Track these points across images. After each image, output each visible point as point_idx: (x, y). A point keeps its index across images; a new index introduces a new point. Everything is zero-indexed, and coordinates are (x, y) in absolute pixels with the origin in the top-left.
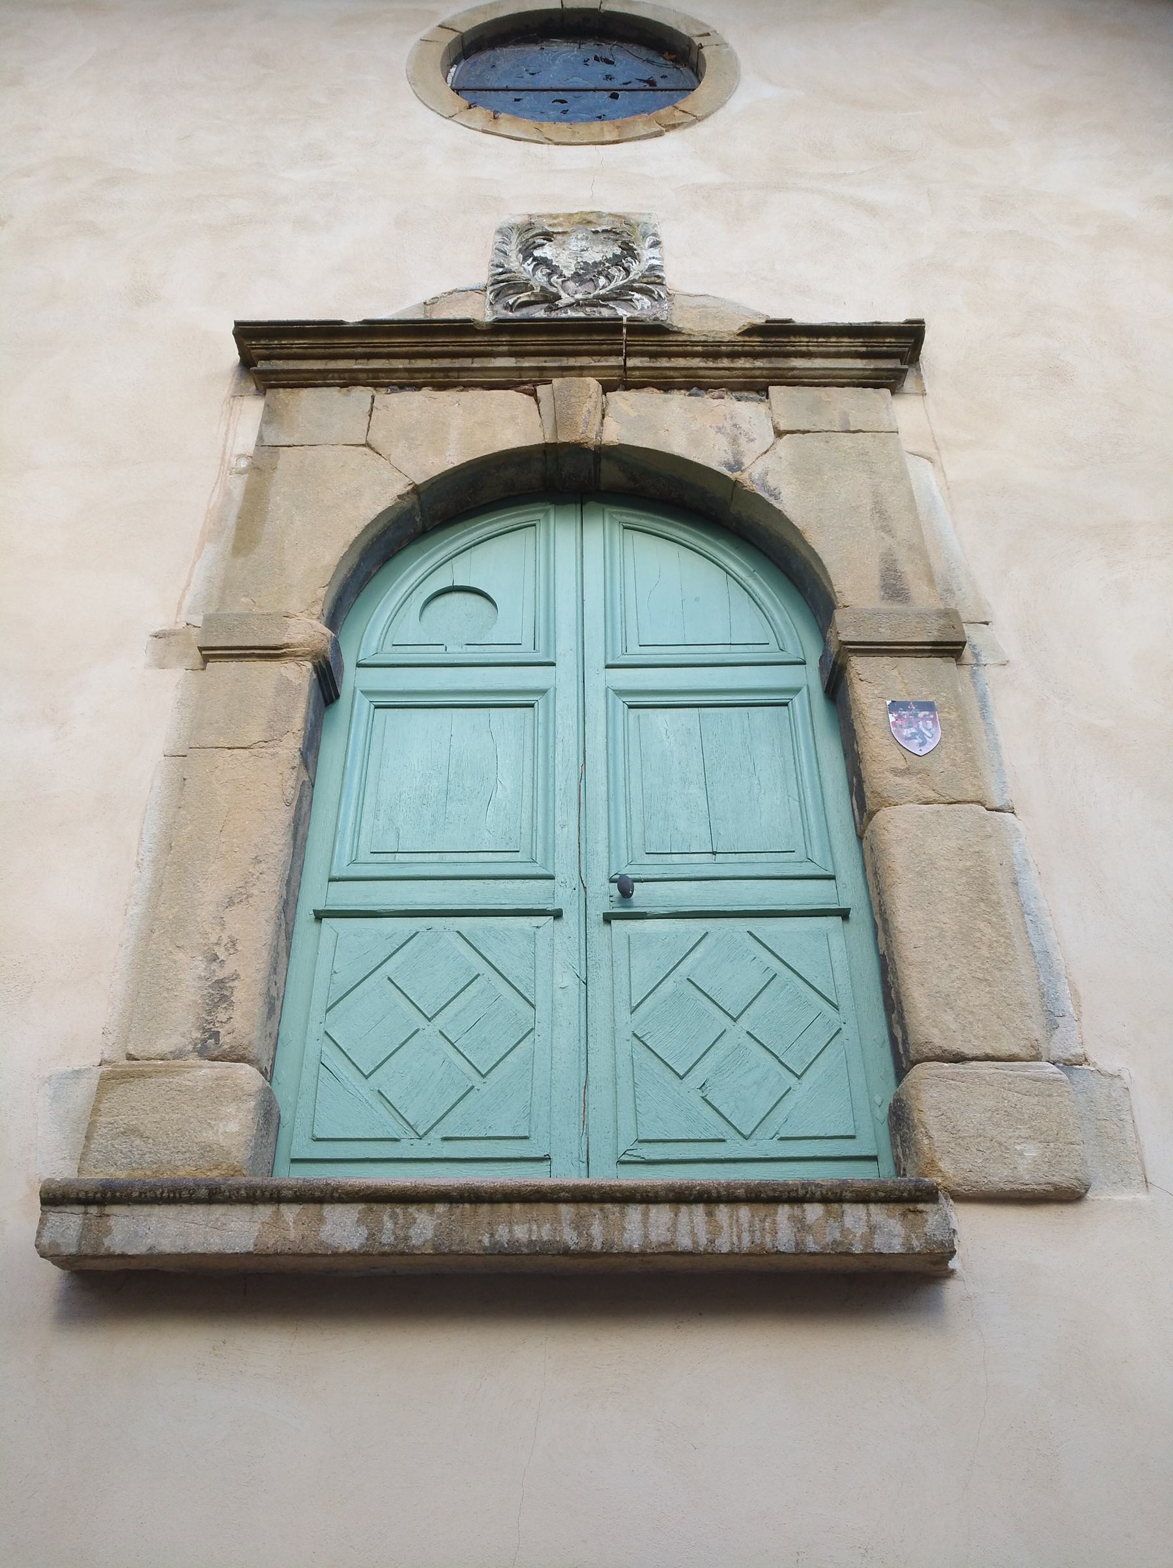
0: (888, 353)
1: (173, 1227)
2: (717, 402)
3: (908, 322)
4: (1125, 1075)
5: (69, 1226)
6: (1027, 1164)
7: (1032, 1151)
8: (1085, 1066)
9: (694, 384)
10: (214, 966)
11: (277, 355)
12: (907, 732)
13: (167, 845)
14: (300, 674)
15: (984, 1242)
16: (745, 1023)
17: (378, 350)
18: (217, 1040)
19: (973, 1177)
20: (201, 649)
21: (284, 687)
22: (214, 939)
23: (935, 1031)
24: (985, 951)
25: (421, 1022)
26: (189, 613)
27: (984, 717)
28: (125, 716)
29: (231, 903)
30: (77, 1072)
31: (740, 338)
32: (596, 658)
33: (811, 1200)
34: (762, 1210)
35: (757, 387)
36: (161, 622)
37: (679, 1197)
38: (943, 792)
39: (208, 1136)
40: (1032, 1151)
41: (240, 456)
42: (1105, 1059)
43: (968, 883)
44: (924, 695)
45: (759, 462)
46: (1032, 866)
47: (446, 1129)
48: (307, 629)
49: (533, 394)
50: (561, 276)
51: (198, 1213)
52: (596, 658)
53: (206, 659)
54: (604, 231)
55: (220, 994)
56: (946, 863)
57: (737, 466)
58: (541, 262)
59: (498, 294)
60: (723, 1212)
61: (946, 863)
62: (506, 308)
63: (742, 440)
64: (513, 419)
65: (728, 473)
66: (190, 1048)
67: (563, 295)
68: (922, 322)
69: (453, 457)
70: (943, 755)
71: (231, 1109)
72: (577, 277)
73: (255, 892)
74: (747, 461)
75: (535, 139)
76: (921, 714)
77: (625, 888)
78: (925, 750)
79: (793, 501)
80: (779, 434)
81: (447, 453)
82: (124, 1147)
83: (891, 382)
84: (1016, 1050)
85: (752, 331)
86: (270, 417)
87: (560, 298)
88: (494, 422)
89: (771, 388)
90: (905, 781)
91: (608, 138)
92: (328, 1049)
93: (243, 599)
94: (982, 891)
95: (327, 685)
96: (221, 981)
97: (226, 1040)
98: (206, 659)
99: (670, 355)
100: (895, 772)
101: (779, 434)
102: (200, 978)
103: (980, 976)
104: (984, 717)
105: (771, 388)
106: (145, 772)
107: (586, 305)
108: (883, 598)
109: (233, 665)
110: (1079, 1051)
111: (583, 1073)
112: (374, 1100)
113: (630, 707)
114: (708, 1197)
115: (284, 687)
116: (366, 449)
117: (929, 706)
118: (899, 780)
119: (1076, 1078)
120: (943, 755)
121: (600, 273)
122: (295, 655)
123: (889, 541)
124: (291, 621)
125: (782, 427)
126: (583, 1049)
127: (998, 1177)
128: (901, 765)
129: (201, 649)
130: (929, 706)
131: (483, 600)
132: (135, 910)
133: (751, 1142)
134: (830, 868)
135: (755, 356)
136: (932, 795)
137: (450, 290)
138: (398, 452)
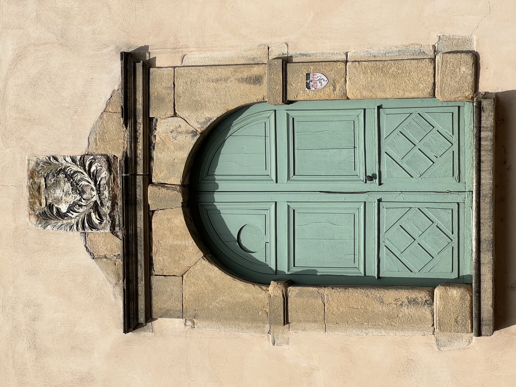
1: (486, 302)
2: (157, 138)
3: (122, 59)
4: (439, 35)
7: (463, 69)
8: (436, 46)
9: (149, 146)
10: (404, 304)
12: (319, 84)
13: (360, 325)
14: (293, 291)
16: (416, 142)
17: (134, 275)
18: (428, 300)
19: (470, 87)
20: (284, 324)
21: (299, 295)
22: (395, 306)
23: (426, 90)
24: (400, 71)
25: (416, 242)
26: (264, 333)
27: (310, 56)
29: (383, 302)
30: (436, 341)
31: (128, 128)
33: (480, 135)
34: (482, 148)
38: (342, 76)
39: (458, 299)
40: (463, 69)
41: (185, 325)
42: (434, 41)
43: (376, 73)
45: (192, 124)
46: (368, 50)
47: (449, 233)
48: (274, 289)
49: (153, 212)
50: (80, 200)
51: (482, 295)
52: (273, 186)
53: (288, 323)
54: (45, 181)
55: (413, 302)
56: (369, 79)
58: (71, 209)
59: (92, 226)
60: (482, 159)
61: (369, 79)
62: (101, 224)
63: (180, 130)
64: (168, 219)
65: (198, 136)
66: (430, 308)
67: (94, 199)
68: (121, 54)
69: (190, 242)
70: (328, 73)
71: (450, 293)
72: (82, 192)
73: (378, 295)
74: (191, 129)
76: (311, 79)
77: (371, 178)
78: (325, 79)
79: (214, 114)
80: (175, 115)
81: (187, 244)
82: (461, 321)
84: (432, 67)
85: (126, 124)
86: (167, 314)
87: (96, 201)
88: (170, 228)
89: (151, 116)
90: (338, 87)
92: (425, 270)
93: (260, 314)
94: (379, 69)
95: (291, 281)
96: (409, 302)
97: (428, 298)
98: (288, 323)
99: (136, 156)
100: (334, 89)
101: (175, 115)
102: (408, 308)
103: (408, 74)
104: (310, 56)
105: (151, 116)
106: (335, 337)
107: (99, 191)
108: (260, 85)
109: (289, 314)
110: (431, 47)
111: (432, 193)
112: (439, 256)
113: (294, 175)
114: (479, 162)
115: (299, 295)
116: (184, 276)
117: (308, 75)
118: (337, 89)
119: (440, 50)
120: (328, 73)
121: (77, 184)
122: (286, 293)
123: (232, 79)
124: (272, 295)
125: (172, 114)
126: (424, 193)
127: (470, 79)
128: (332, 88)
129: (284, 324)
130: (308, 75)
131: (243, 229)
132: (383, 332)
133: (453, 143)
134: (361, 110)
135: (135, 122)
136: (343, 79)
137: (85, 249)
138: (185, 264)
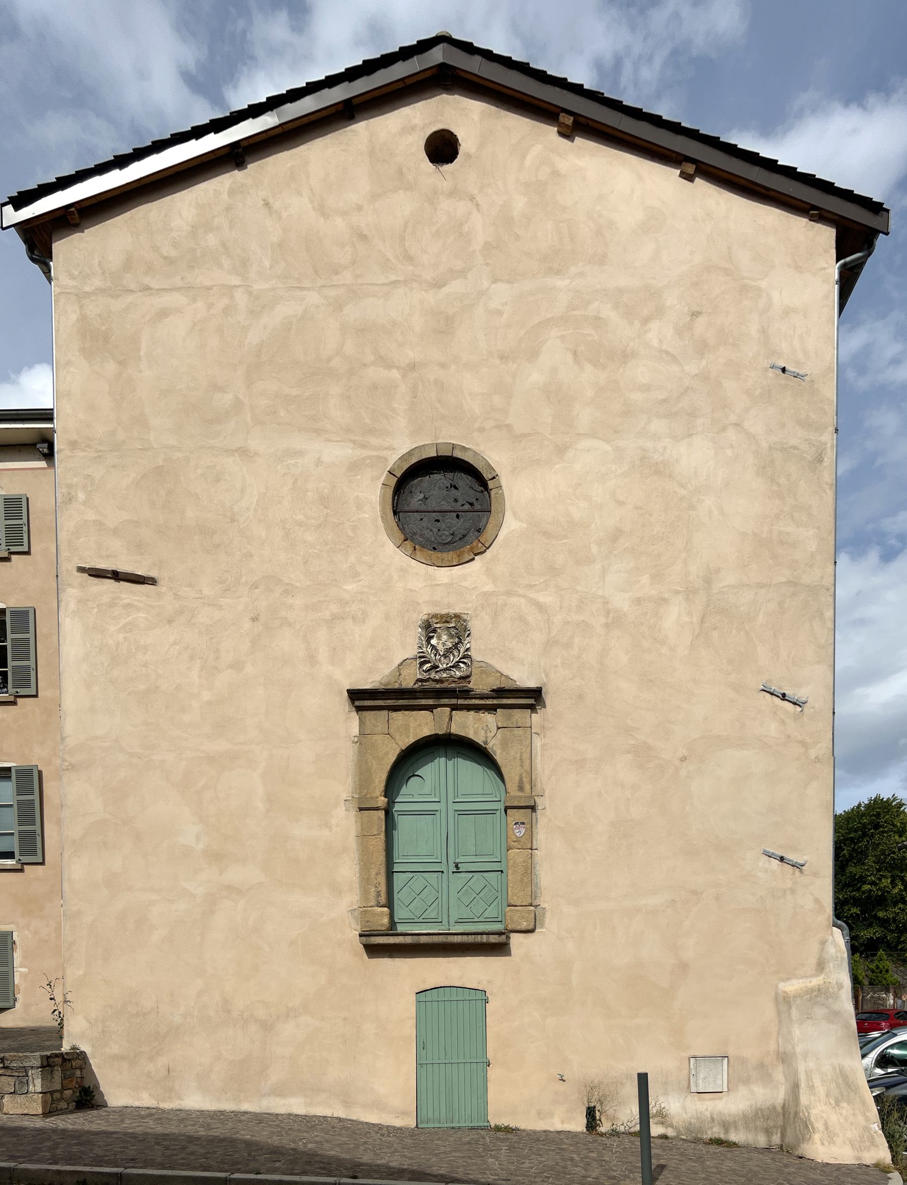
0: (533, 698)
5: (364, 939)
6: (524, 925)
9: (477, 708)
11: (360, 699)
14: (382, 814)
15: (516, 940)
21: (379, 818)
28: (343, 826)
32: (451, 800)
35: (492, 709)
36: (345, 796)
37: (482, 934)
42: (543, 905)
44: (523, 820)
48: (382, 801)
52: (451, 800)
55: (378, 894)
57: (486, 743)
75: (421, 937)
77: (457, 867)
80: (498, 728)
83: (532, 708)
85: (493, 691)
86: (362, 723)
88: (421, 724)
91: (455, 563)
95: (388, 812)
99: (470, 698)
115: (379, 818)
127: (519, 928)
135: (494, 698)
